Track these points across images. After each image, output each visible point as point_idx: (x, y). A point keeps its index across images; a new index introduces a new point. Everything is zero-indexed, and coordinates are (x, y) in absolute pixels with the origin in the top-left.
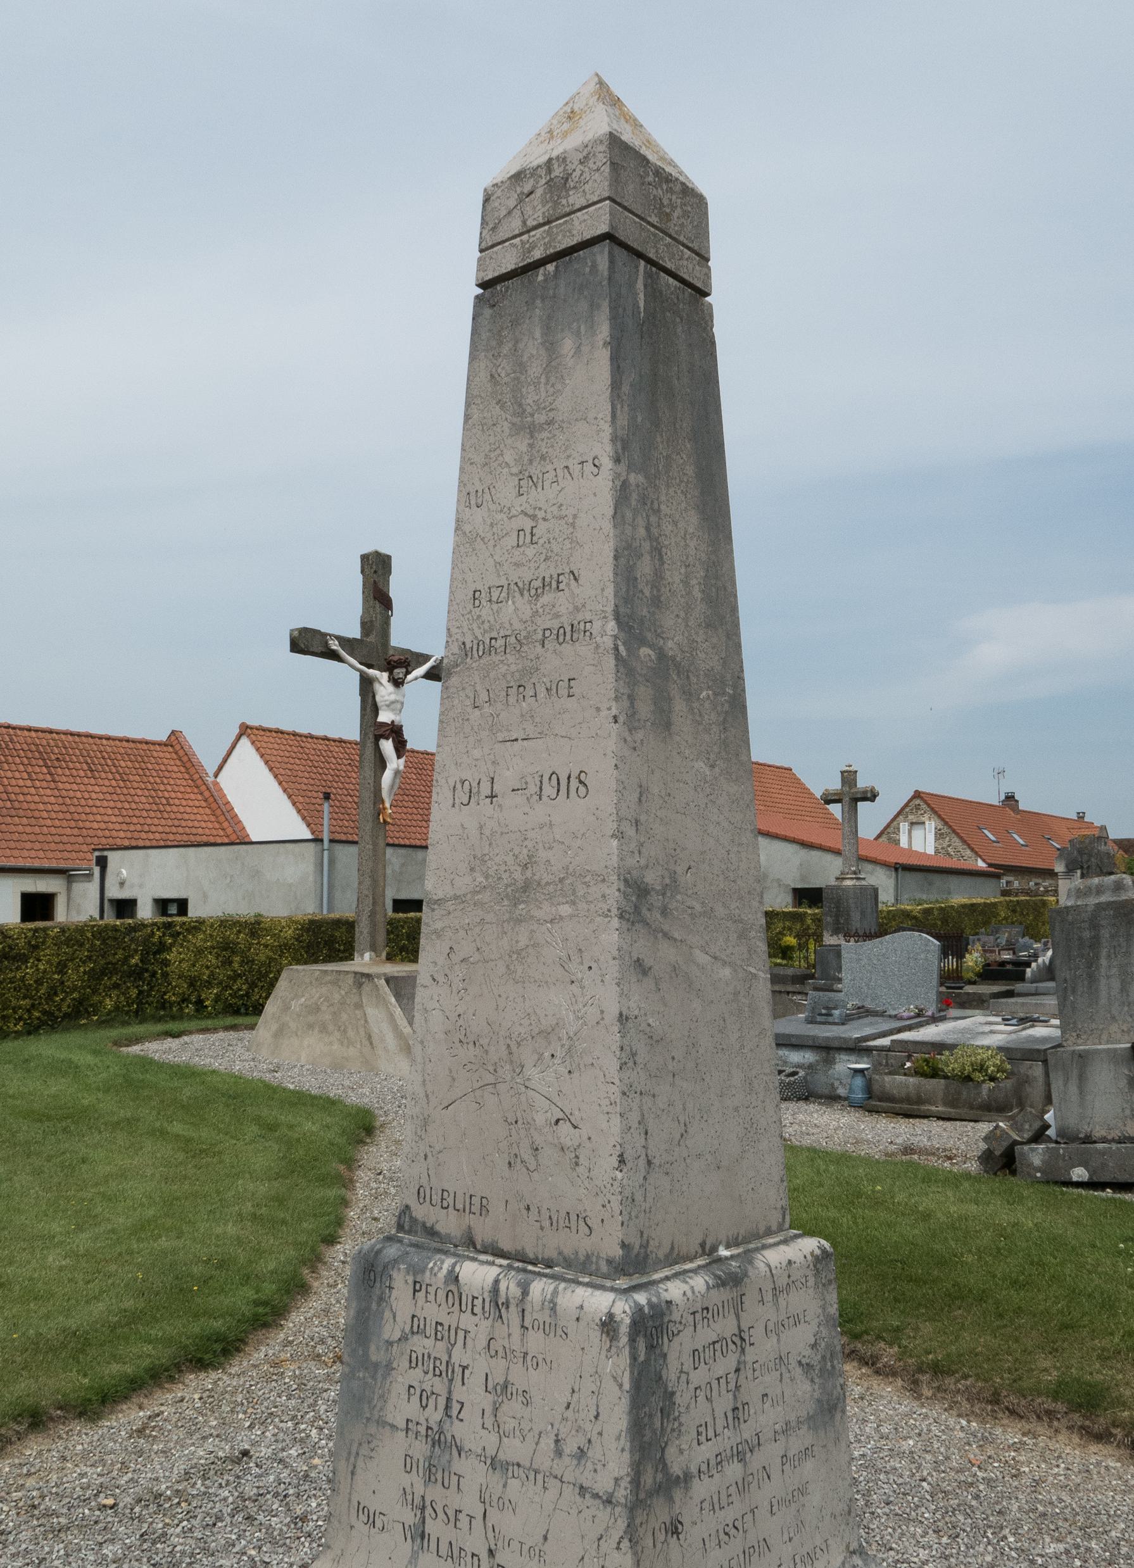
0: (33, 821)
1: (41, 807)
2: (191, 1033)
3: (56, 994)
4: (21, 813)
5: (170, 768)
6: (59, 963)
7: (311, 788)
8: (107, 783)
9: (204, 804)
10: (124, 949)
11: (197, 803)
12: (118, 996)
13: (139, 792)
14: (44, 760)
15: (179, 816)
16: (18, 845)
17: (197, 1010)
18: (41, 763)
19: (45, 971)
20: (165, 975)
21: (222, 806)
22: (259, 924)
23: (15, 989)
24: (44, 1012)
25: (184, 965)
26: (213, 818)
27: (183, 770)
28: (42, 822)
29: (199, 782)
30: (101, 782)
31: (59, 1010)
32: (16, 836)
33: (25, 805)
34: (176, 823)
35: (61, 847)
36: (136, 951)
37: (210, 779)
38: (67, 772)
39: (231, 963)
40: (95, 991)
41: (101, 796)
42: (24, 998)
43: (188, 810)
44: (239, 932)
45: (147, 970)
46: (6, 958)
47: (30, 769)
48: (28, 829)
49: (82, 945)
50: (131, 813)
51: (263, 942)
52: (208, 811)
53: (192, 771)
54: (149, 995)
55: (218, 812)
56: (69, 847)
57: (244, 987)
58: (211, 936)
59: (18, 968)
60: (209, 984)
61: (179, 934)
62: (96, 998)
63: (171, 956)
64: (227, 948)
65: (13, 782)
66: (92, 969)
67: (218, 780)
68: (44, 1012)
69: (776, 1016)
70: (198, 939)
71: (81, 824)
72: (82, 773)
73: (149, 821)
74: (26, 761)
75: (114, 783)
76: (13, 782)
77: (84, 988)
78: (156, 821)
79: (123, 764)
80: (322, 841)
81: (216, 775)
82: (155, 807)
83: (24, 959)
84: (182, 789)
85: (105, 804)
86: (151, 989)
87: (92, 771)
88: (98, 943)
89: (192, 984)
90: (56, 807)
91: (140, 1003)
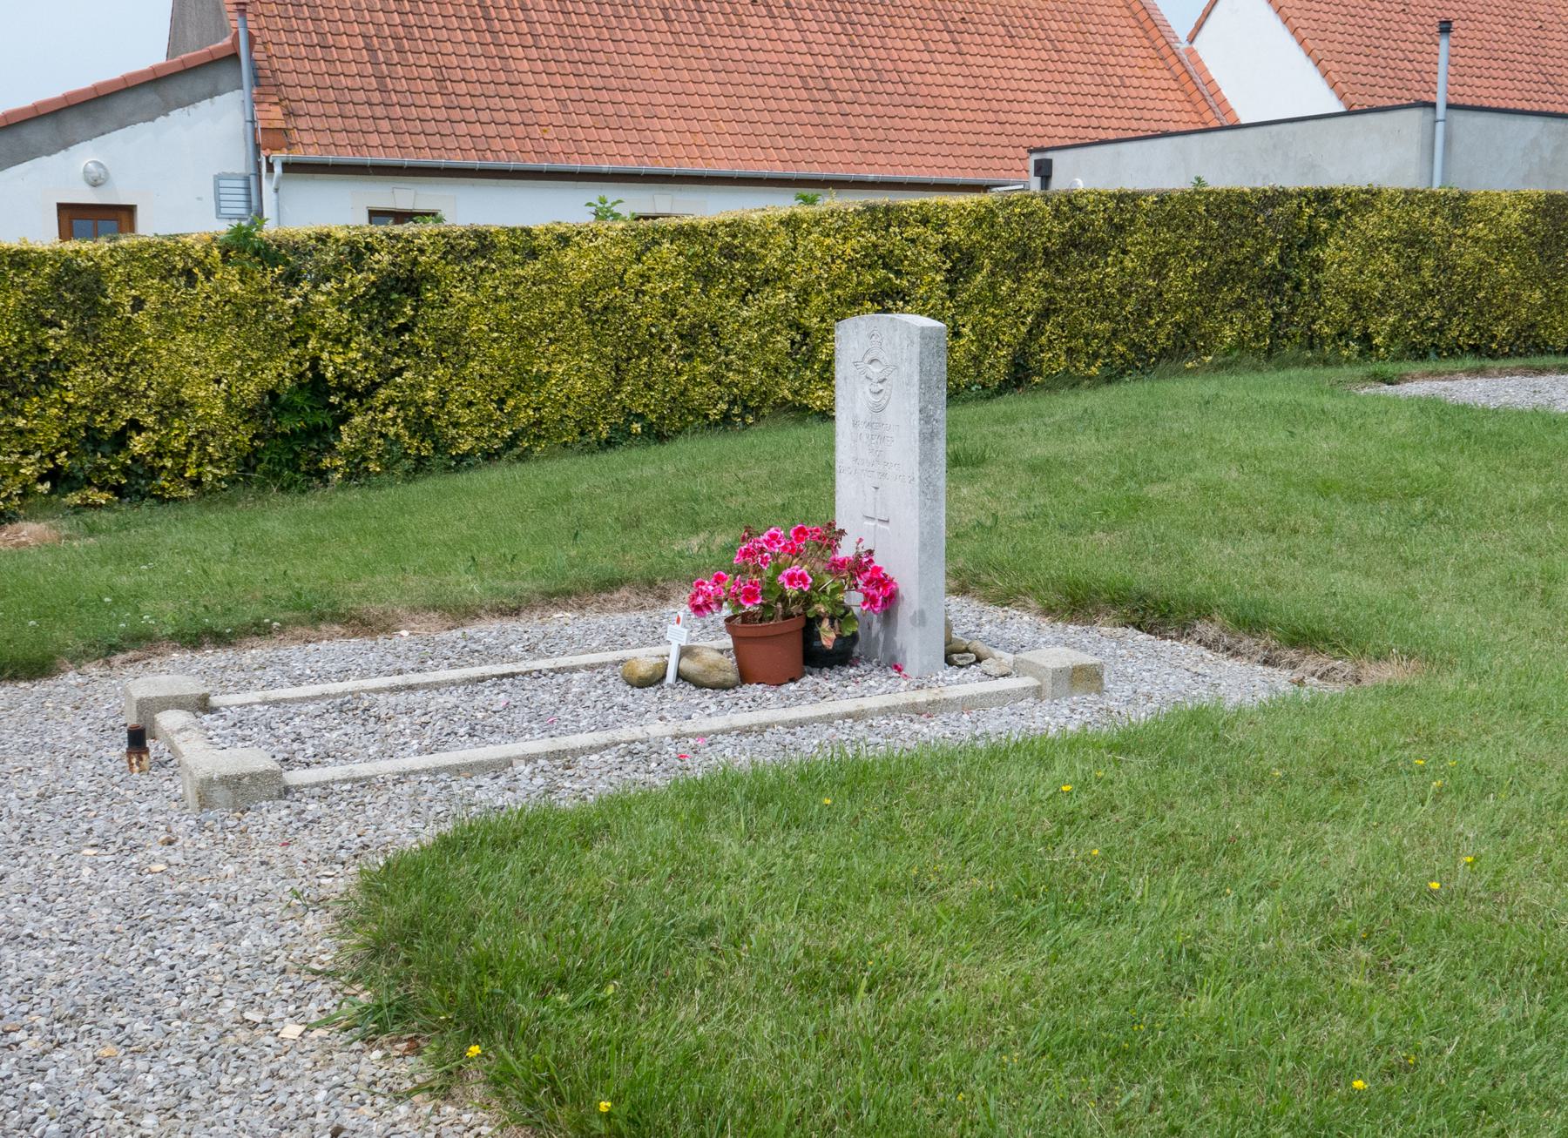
0: (937, 114)
1: (946, 91)
2: (1413, 379)
3: (1149, 314)
4: (920, 101)
5: (1121, 31)
6: (1155, 258)
7: (1348, 48)
8: (1034, 54)
9: (1175, 86)
10: (1255, 237)
11: (1165, 84)
12: (1243, 322)
13: (1081, 68)
14: (944, 21)
15: (1141, 104)
16: (918, 148)
17: (1361, 353)
18: (940, 26)
19: (1134, 273)
20: (1316, 287)
21: (1202, 87)
22: (1466, 200)
23: (1088, 302)
24: (1133, 346)
25: (1345, 271)
26: (1188, 107)
27: (1140, 33)
28: (950, 114)
29: (1165, 51)
30: (1025, 53)
31: (1154, 342)
32: (915, 136)
33: (925, 90)
34: (1137, 114)
35: (978, 151)
36: (1273, 240)
37: (1182, 46)
38: (978, 39)
39: (1418, 269)
40: (1208, 312)
41: (1028, 75)
42: (1103, 318)
43: (1152, 94)
44: (1434, 213)
45: (1288, 278)
46: (1075, 247)
47: (926, 35)
48: (931, 125)
49: (1189, 228)
50: (1071, 100)
51: (1471, 233)
52: (1182, 97)
53: (1154, 33)
54: (1289, 323)
55: (1197, 96)
56: (989, 151)
57: (1437, 314)
58: (1390, 218)
59: (1094, 265)
60: (1381, 307)
61: (1339, 213)
62: (1208, 325)
63: (1327, 253)
64: (1414, 240)
65: (905, 55)
66: (1206, 272)
67: (1195, 45)
68: (1133, 346)
69: (1101, 666)
70: (1369, 224)
71: (1002, 117)
72: (998, 41)
73: (1097, 111)
74: (919, 24)
75: (1044, 55)
76: (905, 55)
77: (1191, 304)
78: (1108, 112)
79: (1054, 25)
80: (1433, 105)
81: (1191, 39)
82: (1104, 90)
83: (1100, 247)
84: (1141, 63)
85: (1034, 86)
86: (1293, 313)
87: (1011, 37)
88: (1216, 224)
89: (1355, 307)
90: (967, 92)
91: (1275, 336)
